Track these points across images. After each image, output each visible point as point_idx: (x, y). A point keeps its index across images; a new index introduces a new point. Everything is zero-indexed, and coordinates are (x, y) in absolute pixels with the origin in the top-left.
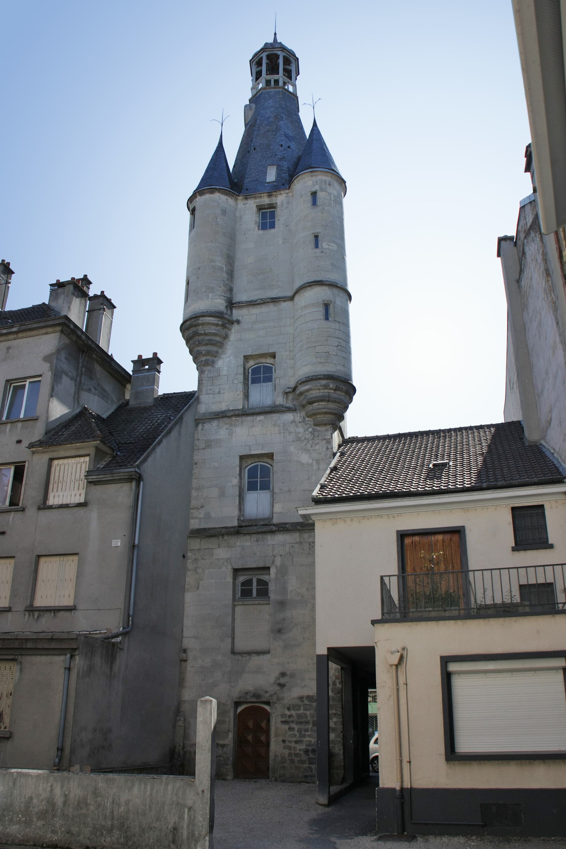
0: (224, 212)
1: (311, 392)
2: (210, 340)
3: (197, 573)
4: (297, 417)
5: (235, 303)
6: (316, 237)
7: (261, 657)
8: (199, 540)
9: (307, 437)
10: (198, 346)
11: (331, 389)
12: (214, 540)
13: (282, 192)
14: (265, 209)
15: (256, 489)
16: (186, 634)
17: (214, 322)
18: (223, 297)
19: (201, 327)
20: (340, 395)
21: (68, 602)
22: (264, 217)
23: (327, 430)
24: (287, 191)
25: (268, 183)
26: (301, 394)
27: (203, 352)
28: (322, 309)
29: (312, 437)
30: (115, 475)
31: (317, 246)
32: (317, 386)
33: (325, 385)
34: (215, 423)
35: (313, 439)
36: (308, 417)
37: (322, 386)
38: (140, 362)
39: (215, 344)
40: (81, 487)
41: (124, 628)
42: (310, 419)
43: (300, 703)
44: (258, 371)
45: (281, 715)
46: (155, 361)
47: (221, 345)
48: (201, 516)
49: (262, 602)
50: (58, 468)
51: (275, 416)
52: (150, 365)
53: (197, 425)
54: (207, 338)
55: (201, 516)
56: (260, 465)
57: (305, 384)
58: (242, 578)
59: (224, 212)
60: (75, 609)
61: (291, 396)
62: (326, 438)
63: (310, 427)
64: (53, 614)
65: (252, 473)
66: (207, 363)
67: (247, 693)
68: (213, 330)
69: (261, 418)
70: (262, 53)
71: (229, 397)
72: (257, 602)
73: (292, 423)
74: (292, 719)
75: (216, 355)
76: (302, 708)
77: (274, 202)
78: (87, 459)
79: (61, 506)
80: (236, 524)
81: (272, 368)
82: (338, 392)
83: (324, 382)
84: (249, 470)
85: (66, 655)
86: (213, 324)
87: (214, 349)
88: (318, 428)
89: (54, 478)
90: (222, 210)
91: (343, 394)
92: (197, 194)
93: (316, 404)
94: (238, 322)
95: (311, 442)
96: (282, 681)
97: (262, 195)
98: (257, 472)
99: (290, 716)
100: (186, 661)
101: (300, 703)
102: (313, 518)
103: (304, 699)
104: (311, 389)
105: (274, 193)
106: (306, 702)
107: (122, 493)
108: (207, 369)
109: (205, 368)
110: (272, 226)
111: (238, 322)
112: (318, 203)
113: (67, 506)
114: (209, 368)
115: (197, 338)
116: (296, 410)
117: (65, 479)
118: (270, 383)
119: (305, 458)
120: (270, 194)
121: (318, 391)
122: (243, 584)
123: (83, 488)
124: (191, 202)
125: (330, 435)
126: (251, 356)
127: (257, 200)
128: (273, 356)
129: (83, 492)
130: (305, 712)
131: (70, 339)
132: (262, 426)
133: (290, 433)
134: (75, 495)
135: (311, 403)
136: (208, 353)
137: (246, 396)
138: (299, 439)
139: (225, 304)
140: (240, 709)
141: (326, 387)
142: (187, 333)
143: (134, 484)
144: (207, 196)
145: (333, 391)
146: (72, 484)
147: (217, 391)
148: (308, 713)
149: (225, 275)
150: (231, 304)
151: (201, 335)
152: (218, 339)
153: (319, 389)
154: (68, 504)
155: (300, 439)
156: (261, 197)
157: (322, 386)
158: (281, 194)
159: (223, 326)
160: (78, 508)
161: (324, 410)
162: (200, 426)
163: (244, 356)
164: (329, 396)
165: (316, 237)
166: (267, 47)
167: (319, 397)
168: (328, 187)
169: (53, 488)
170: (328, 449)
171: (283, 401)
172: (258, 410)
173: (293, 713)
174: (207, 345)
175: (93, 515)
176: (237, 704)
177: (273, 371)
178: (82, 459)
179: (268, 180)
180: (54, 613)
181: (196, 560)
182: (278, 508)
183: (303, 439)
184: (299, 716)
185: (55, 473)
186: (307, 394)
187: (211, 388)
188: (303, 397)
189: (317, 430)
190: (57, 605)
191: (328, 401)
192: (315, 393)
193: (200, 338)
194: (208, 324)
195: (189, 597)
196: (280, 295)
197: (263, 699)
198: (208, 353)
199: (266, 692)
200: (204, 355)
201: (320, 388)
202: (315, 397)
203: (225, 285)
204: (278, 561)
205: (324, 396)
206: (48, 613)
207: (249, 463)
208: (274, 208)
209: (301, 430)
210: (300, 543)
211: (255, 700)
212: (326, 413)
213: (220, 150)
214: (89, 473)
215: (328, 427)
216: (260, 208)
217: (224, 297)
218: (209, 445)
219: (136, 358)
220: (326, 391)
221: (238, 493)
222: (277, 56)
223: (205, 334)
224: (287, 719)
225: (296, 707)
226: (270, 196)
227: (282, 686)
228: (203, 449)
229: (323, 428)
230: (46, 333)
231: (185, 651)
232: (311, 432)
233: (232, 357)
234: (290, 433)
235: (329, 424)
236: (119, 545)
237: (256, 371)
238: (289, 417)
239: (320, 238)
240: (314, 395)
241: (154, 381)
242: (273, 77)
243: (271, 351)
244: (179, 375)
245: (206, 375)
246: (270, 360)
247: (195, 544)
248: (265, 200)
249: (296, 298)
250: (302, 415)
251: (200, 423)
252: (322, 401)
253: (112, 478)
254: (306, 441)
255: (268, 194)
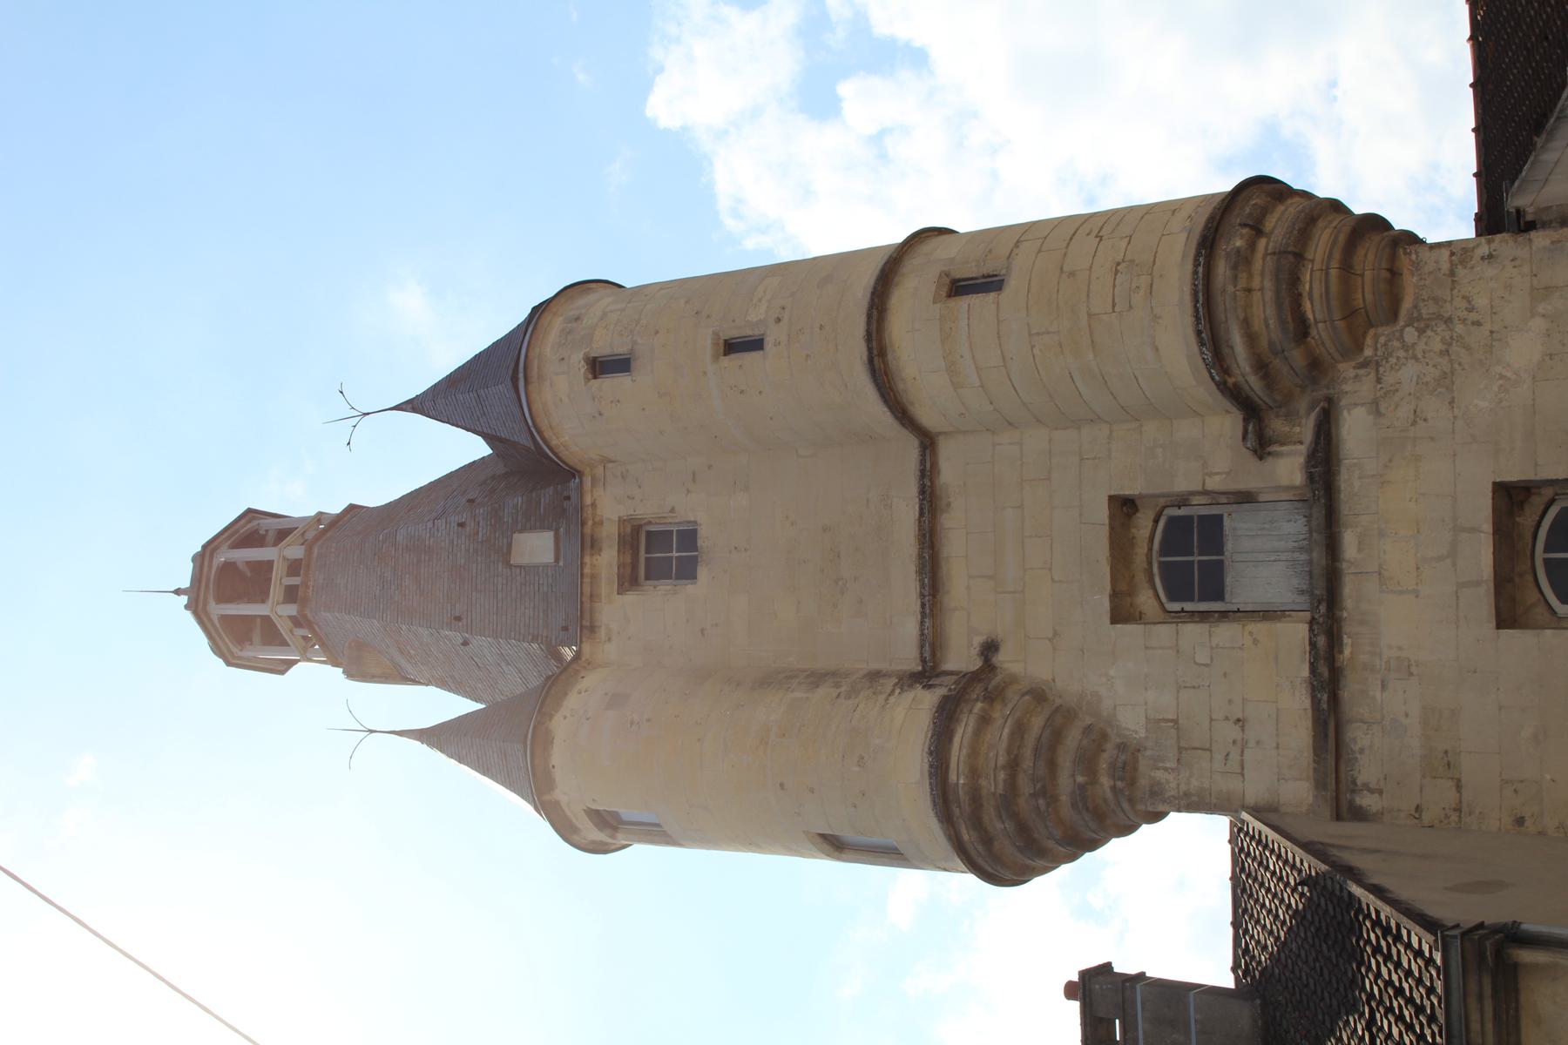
1: (1257, 325)
2: (1037, 750)
5: (923, 661)
9: (1437, 345)
10: (1053, 799)
11: (1252, 246)
13: (588, 500)
14: (634, 566)
17: (970, 729)
18: (892, 699)
19: (983, 782)
20: (1279, 222)
22: (657, 572)
23: (1417, 265)
25: (557, 560)
26: (1262, 367)
27: (1080, 779)
29: (1441, 327)
32: (1235, 298)
33: (1235, 267)
34: (1359, 737)
35: (1448, 321)
36: (1360, 348)
37: (1235, 278)
39: (1056, 736)
42: (1369, 341)
44: (1175, 559)
47: (1061, 718)
51: (1350, 482)
53: (1359, 815)
54: (1027, 763)
56: (1546, 551)
57: (1226, 351)
61: (1277, 425)
62: (1445, 267)
63: (1401, 338)
66: (1126, 770)
68: (999, 736)
70: (206, 613)
73: (1378, 413)
75: (1098, 737)
83: (1222, 269)
86: (978, 732)
88: (1407, 305)
91: (1281, 208)
92: (546, 797)
93: (1307, 306)
94: (990, 648)
95: (1459, 328)
97: (587, 570)
104: (1246, 323)
105: (588, 530)
108: (1147, 774)
109: (1143, 782)
110: (689, 537)
111: (990, 648)
112: (621, 348)
114: (1143, 766)
115: (1023, 804)
118: (1227, 522)
119: (1523, 350)
120: (588, 543)
121: (1257, 296)
125: (1436, 252)
128: (1124, 507)
132: (1381, 534)
133: (1417, 417)
135: (1301, 330)
136: (1087, 761)
137: (1268, 614)
138: (1445, 381)
139: (918, 691)
141: (1242, 261)
143: (1526, 956)
145: (1262, 242)
147: (1233, 732)
150: (926, 675)
151: (1012, 783)
152: (1037, 723)
153: (1249, 290)
156: (593, 576)
157: (1235, 278)
158: (593, 505)
159: (991, 698)
161: (1333, 272)
162: (1367, 801)
163: (1114, 621)
164: (1280, 254)
166: (197, 607)
167: (1277, 292)
170: (1490, 256)
171: (1290, 454)
172: (1318, 555)
174: (1052, 765)
177: (1183, 512)
179: (549, 558)
183: (1444, 361)
186: (1264, 343)
187: (1219, 757)
188: (1277, 362)
189: (1415, 307)
191: (1299, 257)
192: (1264, 310)
193: (1025, 786)
194: (974, 753)
198: (1087, 761)
201: (1242, 283)
203: (853, 692)
207: (1533, 596)
208: (637, 529)
209: (1408, 374)
212: (1346, 267)
213: (439, 737)
215: (1404, 262)
217: (892, 692)
218: (1446, 765)
220: (1258, 264)
222: (229, 567)
223: (1013, 765)
228: (1459, 787)
229: (1410, 282)
232: (1421, 331)
233: (1112, 673)
234: (1417, 417)
238: (1354, 428)
239: (733, 333)
240: (1271, 311)
242: (279, 580)
243: (1102, 513)
245: (1170, 777)
246: (1143, 525)
248: (607, 561)
249: (927, 417)
250: (1351, 373)
251: (1351, 803)
252: (1295, 281)
254: (1455, 348)
255: (588, 551)
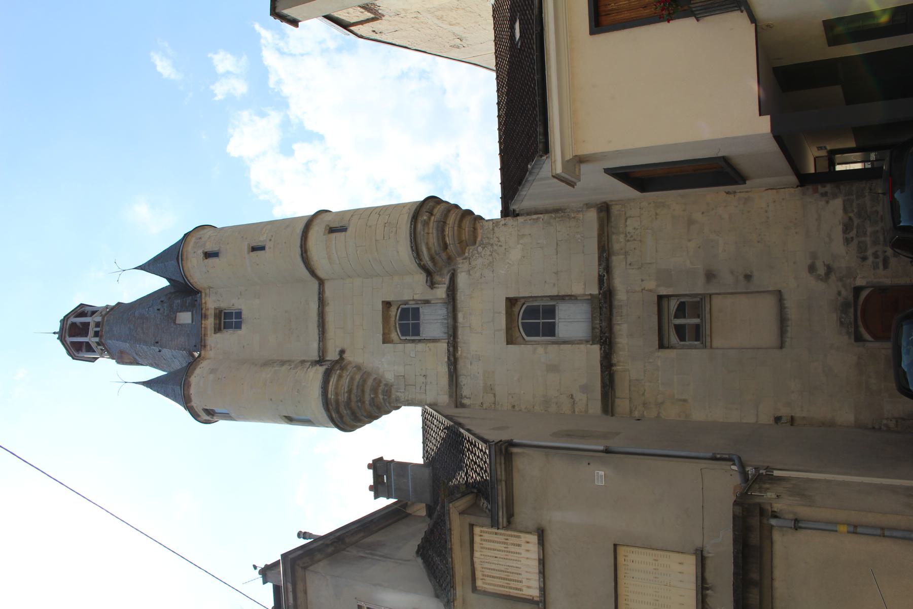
0: (213, 371)
1: (431, 245)
3: (662, 403)
4: (462, 267)
6: (254, 249)
7: (788, 303)
8: (617, 400)
9: (489, 253)
10: (363, 403)
11: (429, 219)
12: (617, 378)
15: (554, 324)
16: (751, 419)
21: (690, 564)
22: (228, 326)
23: (482, 226)
24: (203, 294)
26: (432, 259)
28: (334, 235)
30: (499, 477)
31: (262, 248)
34: (463, 380)
35: (492, 245)
36: (464, 253)
38: (378, 489)
40: (515, 540)
41: (734, 464)
43: (855, 242)
44: (404, 321)
45: (874, 269)
46: (380, 467)
47: (366, 375)
48: (584, 397)
49: (708, 309)
50: (488, 580)
52: (384, 473)
53: (463, 406)
54: (355, 391)
55: (584, 397)
58: (674, 339)
59: (213, 371)
60: (702, 551)
61: (437, 278)
64: (709, 592)
65: (532, 330)
66: (388, 392)
67: (841, 323)
68: (345, 381)
69: (460, 316)
71: (429, 360)
72: (708, 316)
74: (880, 253)
76: (863, 239)
77: (213, 312)
78: (477, 530)
79: (543, 572)
80: (596, 348)
81: (403, 309)
82: (435, 211)
83: (419, 226)
84: (528, 336)
85: (772, 526)
87: (370, 382)
88: (479, 239)
89: (503, 586)
90: (211, 373)
94: (342, 352)
95: (495, 247)
96: (821, 271)
98: (531, 319)
99: (876, 255)
100: (792, 418)
101: (855, 242)
102: (569, 156)
103: (848, 236)
104: (427, 244)
106: (853, 233)
107: (529, 470)
109: (393, 396)
110: (239, 314)
111: (342, 352)
113: (542, 562)
114: (393, 391)
115: (353, 405)
116: (454, 270)
117: (502, 568)
118: (421, 310)
122: (682, 338)
123: (519, 537)
124: (199, 416)
126: (384, 334)
127: (209, 332)
128: (387, 305)
129: (525, 537)
130: (868, 233)
131: (320, 561)
132: (470, 314)
134: (527, 550)
135: (445, 247)
136: (375, 390)
137: (434, 340)
138: (491, 264)
139: (318, 367)
140: (867, 336)
141: (426, 224)
142: (347, 419)
143: (515, 450)
144: (193, 391)
146: (511, 556)
147: (422, 379)
148: (869, 230)
149: (284, 368)
150: (320, 361)
151: (349, 398)
152: (358, 377)
154: (539, 560)
155: (490, 262)
159: (342, 369)
160: (547, 545)
162: (465, 401)
164: (438, 222)
165: (254, 249)
168: (203, 239)
169: (517, 589)
172: (450, 321)
173: (870, 252)
175: (558, 519)
176: (858, 338)
178: (477, 539)
180: (708, 589)
181: (644, 404)
182: (577, 290)
183: (490, 258)
184: (875, 243)
185: (495, 585)
186: (433, 251)
188: (437, 257)
190: (694, 587)
191: (445, 223)
192: (433, 240)
194: (337, 387)
195: (698, 415)
196: (316, 299)
197: (851, 298)
199: (839, 293)
200: (377, 396)
201: (426, 231)
202: (438, 239)
204: (651, 284)
205: (438, 227)
206: (708, 600)
209: (479, 261)
210: (626, 254)
211: (852, 310)
212: (460, 226)
213: (150, 384)
214: (495, 524)
216: (218, 329)
218: (490, 389)
219: (372, 493)
220: (431, 224)
221: (556, 346)
223: (350, 391)
224: (880, 261)
225: (862, 248)
226: (205, 317)
227: (829, 270)
230: (305, 592)
231: (778, 419)
232: (483, 248)
235: (475, 224)
236: (603, 473)
237: (405, 330)
238: (462, 279)
239: (255, 244)
240: (435, 240)
241: (403, 467)
243: (380, 307)
244: (401, 435)
246: (393, 311)
247: (622, 405)
248: (210, 322)
252: (443, 230)
253: (504, 483)
